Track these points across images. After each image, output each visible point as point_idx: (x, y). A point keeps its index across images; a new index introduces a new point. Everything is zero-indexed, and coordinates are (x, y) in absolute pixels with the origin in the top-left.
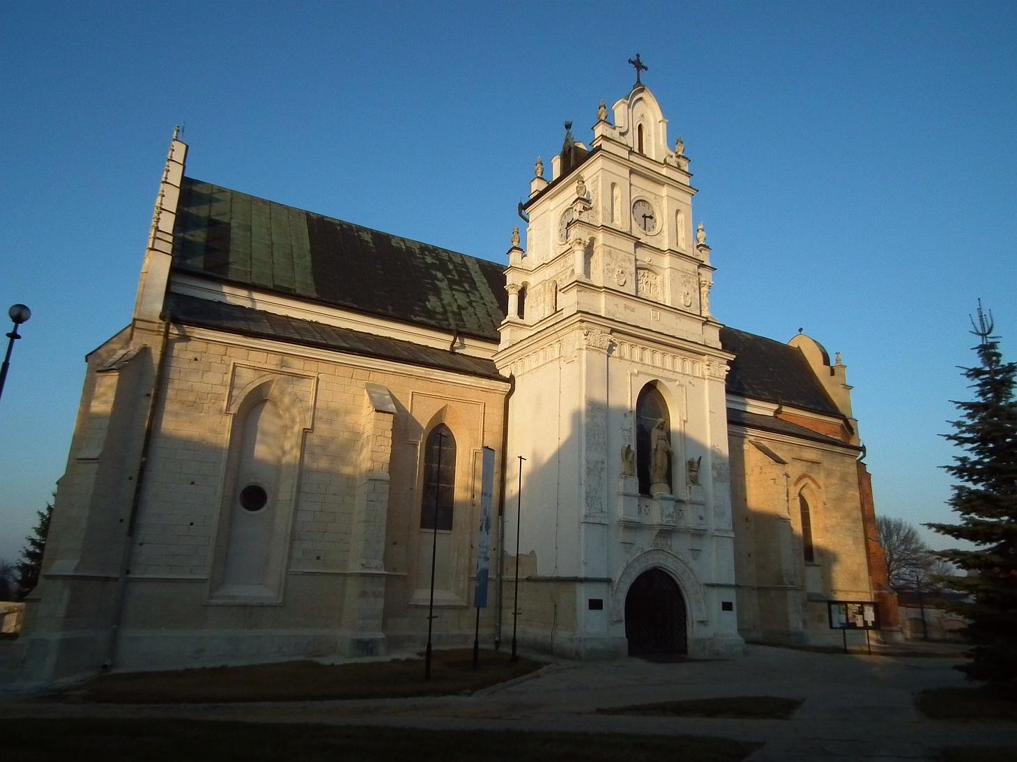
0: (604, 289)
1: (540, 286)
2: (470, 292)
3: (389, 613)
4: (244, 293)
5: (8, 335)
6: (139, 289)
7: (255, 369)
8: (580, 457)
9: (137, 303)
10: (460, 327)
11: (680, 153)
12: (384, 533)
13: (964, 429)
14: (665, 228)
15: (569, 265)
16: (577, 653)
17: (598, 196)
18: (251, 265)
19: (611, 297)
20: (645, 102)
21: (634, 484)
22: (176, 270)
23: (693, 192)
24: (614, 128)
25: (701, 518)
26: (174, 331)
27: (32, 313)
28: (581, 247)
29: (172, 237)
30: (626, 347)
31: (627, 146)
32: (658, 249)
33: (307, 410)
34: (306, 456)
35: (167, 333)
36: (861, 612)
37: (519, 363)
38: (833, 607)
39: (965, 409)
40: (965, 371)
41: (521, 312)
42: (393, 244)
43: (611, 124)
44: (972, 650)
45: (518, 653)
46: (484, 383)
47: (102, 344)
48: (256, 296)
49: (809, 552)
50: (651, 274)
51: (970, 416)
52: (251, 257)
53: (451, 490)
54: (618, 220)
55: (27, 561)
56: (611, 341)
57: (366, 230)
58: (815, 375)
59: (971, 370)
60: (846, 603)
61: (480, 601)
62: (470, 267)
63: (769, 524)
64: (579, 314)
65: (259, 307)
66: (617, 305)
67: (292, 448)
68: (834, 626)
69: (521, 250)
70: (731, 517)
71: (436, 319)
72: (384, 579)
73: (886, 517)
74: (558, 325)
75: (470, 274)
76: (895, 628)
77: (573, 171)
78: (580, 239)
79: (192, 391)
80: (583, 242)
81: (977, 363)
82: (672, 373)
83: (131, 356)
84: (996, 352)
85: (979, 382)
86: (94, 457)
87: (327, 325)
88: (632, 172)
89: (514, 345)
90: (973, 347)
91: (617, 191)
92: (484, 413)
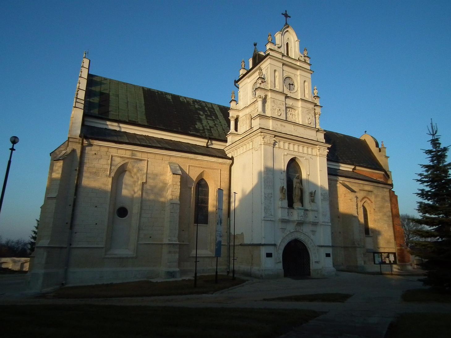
0: (271, 118)
1: (244, 117)
2: (215, 120)
3: (181, 261)
4: (116, 124)
5: (10, 149)
6: (70, 124)
7: (121, 157)
8: (261, 192)
9: (69, 130)
10: (210, 136)
11: (306, 55)
12: (178, 226)
13: (423, 177)
14: (299, 89)
15: (256, 107)
16: (262, 276)
17: (268, 76)
19: (274, 121)
20: (289, 32)
21: (285, 203)
22: (85, 116)
23: (312, 72)
24: (275, 45)
25: (316, 217)
26: (85, 142)
27: (19, 140)
28: (261, 99)
29: (84, 101)
30: (281, 143)
31: (281, 53)
32: (296, 99)
33: (144, 174)
34: (144, 194)
35: (83, 143)
36: (388, 257)
37: (236, 151)
38: (376, 255)
39: (424, 168)
40: (424, 151)
41: (236, 129)
43: (274, 43)
44: (427, 273)
45: (235, 276)
46: (220, 160)
47: (57, 147)
48: (121, 125)
49: (367, 231)
50: (293, 110)
51: (427, 171)
52: (119, 108)
53: (207, 207)
54: (278, 86)
55: (33, 240)
56: (274, 141)
57: (169, 94)
58: (372, 152)
59: (427, 151)
60: (381, 253)
61: (218, 253)
63: (349, 218)
64: (260, 129)
65: (123, 130)
67: (138, 191)
68: (376, 263)
69: (236, 101)
70: (330, 217)
71: (200, 132)
72: (178, 246)
73: (407, 215)
74: (251, 134)
75: (215, 112)
76: (407, 264)
77: (257, 65)
78: (260, 96)
79: (94, 167)
80: (261, 97)
81: (430, 147)
82: (302, 154)
83: (68, 153)
84: (438, 143)
85: (431, 156)
86: (55, 197)
87: (152, 137)
88: (283, 64)
89: (233, 143)
90: (428, 140)
91: (277, 74)
92: (221, 174)
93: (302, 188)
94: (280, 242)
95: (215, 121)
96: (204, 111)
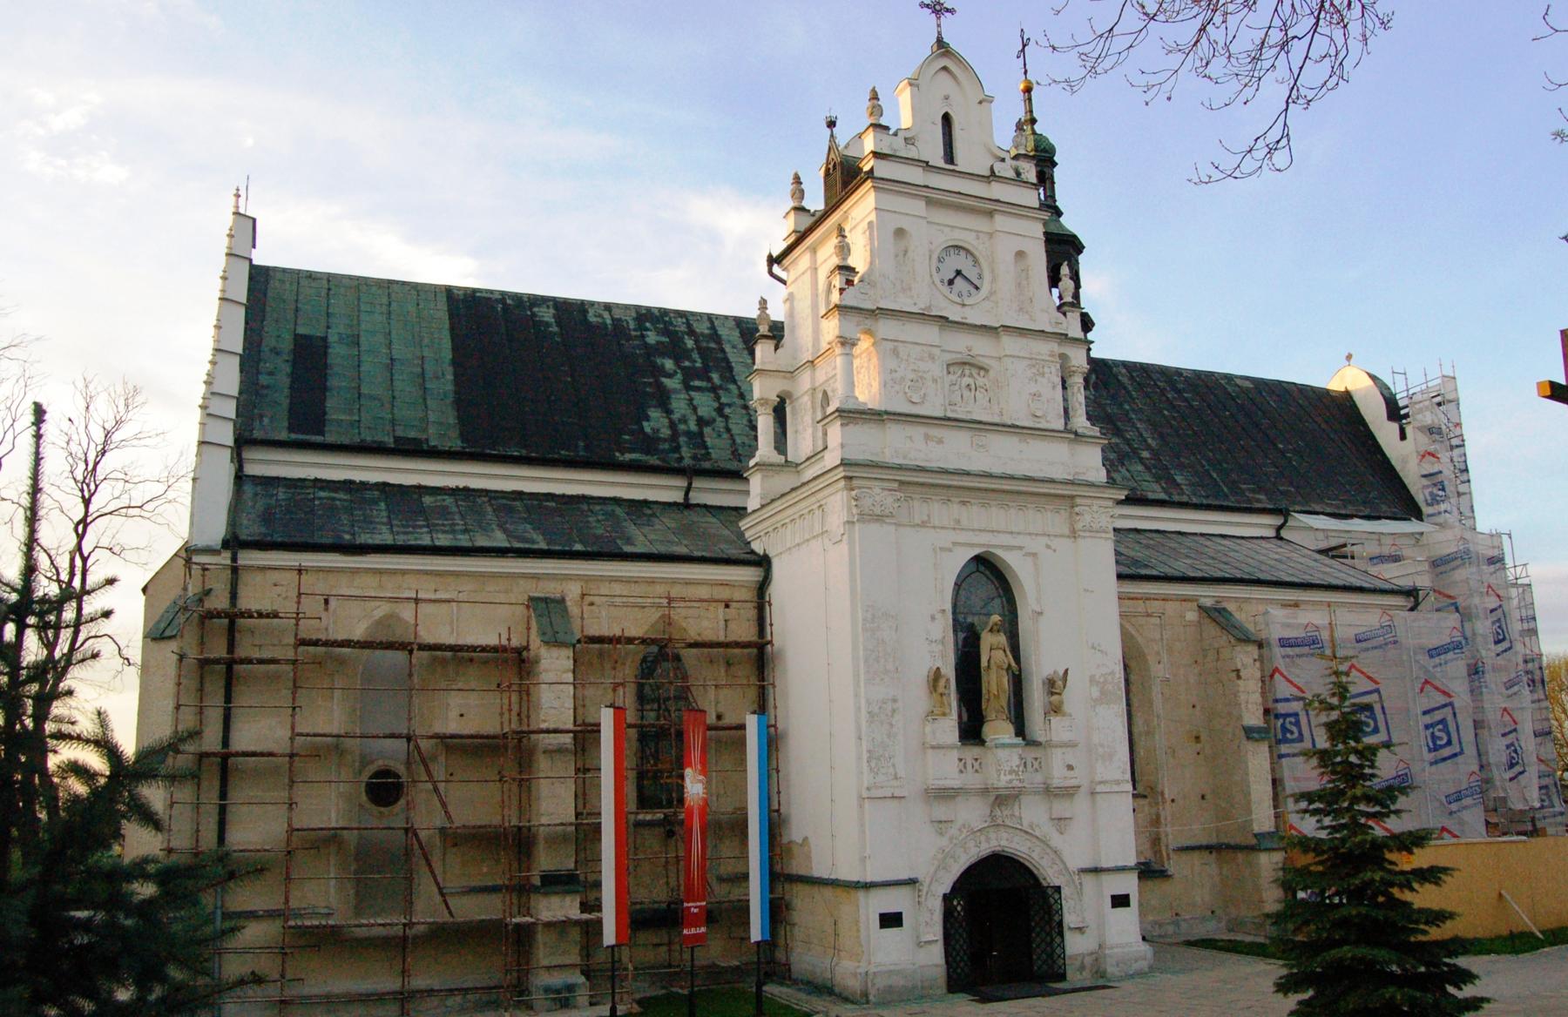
2: (721, 387)
18: (359, 409)
42: (591, 320)
57: (543, 300)
62: (724, 337)
66: (910, 438)
95: (721, 392)
96: (678, 353)
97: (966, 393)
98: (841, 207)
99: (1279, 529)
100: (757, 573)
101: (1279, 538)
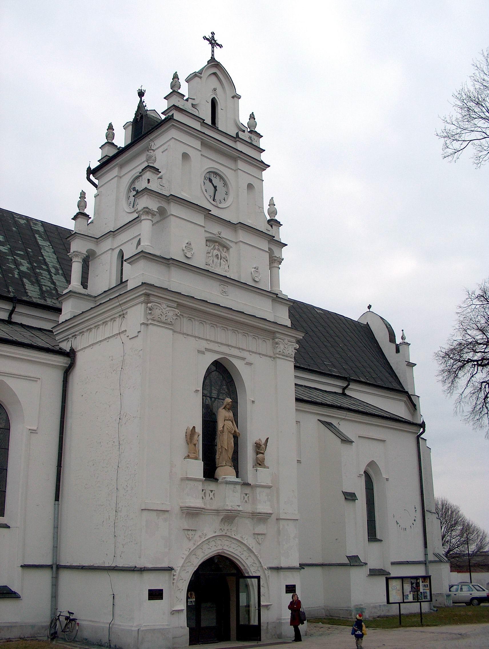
41: (84, 284)
73: (486, 532)
93: (237, 431)
94: (181, 562)
97: (215, 260)
98: (149, 136)
99: (344, 389)
100: (65, 361)
101: (344, 394)
